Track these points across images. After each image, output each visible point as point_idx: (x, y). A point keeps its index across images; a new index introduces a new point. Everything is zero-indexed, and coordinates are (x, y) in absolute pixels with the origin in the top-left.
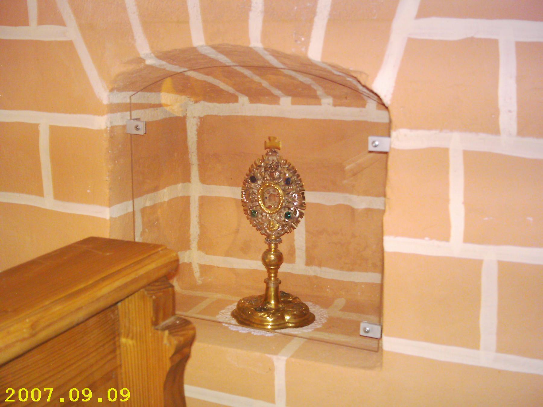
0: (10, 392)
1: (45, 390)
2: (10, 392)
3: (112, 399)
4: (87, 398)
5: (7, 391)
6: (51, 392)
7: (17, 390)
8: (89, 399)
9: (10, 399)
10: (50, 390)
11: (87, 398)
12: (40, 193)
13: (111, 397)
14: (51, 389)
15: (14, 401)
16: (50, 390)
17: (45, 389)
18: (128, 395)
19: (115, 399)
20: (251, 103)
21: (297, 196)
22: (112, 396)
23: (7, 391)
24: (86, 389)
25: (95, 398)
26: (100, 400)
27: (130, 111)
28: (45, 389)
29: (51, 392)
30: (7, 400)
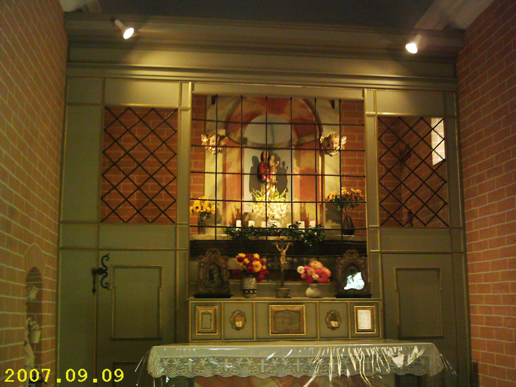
0: (10, 373)
1: (43, 371)
2: (10, 373)
3: (71, 380)
4: (119, 378)
5: (7, 372)
6: (48, 373)
7: (16, 372)
8: (121, 379)
9: (9, 380)
10: (47, 371)
11: (119, 378)
12: (27, 246)
13: (69, 378)
14: (49, 370)
15: (13, 381)
16: (47, 371)
17: (43, 370)
18: (122, 375)
19: (109, 380)
20: (253, 156)
21: (196, 212)
22: (107, 377)
23: (7, 372)
24: (81, 370)
25: (90, 378)
26: (59, 381)
27: (205, 173)
28: (43, 370)
29: (48, 373)
30: (7, 381)
